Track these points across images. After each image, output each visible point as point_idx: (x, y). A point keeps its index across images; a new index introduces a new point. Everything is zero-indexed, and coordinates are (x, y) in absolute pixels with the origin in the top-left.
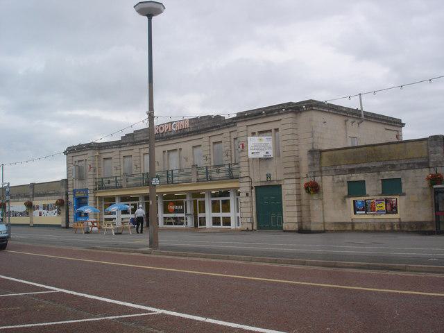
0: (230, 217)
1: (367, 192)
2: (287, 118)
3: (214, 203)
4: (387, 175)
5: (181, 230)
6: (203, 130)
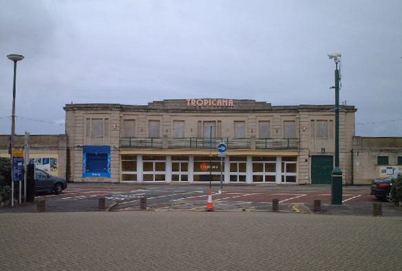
0: (295, 176)
1: (390, 163)
2: (116, 115)
3: (232, 165)
4: (382, 154)
5: (163, 184)
6: (153, 110)
